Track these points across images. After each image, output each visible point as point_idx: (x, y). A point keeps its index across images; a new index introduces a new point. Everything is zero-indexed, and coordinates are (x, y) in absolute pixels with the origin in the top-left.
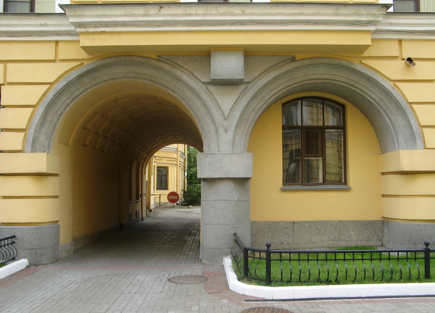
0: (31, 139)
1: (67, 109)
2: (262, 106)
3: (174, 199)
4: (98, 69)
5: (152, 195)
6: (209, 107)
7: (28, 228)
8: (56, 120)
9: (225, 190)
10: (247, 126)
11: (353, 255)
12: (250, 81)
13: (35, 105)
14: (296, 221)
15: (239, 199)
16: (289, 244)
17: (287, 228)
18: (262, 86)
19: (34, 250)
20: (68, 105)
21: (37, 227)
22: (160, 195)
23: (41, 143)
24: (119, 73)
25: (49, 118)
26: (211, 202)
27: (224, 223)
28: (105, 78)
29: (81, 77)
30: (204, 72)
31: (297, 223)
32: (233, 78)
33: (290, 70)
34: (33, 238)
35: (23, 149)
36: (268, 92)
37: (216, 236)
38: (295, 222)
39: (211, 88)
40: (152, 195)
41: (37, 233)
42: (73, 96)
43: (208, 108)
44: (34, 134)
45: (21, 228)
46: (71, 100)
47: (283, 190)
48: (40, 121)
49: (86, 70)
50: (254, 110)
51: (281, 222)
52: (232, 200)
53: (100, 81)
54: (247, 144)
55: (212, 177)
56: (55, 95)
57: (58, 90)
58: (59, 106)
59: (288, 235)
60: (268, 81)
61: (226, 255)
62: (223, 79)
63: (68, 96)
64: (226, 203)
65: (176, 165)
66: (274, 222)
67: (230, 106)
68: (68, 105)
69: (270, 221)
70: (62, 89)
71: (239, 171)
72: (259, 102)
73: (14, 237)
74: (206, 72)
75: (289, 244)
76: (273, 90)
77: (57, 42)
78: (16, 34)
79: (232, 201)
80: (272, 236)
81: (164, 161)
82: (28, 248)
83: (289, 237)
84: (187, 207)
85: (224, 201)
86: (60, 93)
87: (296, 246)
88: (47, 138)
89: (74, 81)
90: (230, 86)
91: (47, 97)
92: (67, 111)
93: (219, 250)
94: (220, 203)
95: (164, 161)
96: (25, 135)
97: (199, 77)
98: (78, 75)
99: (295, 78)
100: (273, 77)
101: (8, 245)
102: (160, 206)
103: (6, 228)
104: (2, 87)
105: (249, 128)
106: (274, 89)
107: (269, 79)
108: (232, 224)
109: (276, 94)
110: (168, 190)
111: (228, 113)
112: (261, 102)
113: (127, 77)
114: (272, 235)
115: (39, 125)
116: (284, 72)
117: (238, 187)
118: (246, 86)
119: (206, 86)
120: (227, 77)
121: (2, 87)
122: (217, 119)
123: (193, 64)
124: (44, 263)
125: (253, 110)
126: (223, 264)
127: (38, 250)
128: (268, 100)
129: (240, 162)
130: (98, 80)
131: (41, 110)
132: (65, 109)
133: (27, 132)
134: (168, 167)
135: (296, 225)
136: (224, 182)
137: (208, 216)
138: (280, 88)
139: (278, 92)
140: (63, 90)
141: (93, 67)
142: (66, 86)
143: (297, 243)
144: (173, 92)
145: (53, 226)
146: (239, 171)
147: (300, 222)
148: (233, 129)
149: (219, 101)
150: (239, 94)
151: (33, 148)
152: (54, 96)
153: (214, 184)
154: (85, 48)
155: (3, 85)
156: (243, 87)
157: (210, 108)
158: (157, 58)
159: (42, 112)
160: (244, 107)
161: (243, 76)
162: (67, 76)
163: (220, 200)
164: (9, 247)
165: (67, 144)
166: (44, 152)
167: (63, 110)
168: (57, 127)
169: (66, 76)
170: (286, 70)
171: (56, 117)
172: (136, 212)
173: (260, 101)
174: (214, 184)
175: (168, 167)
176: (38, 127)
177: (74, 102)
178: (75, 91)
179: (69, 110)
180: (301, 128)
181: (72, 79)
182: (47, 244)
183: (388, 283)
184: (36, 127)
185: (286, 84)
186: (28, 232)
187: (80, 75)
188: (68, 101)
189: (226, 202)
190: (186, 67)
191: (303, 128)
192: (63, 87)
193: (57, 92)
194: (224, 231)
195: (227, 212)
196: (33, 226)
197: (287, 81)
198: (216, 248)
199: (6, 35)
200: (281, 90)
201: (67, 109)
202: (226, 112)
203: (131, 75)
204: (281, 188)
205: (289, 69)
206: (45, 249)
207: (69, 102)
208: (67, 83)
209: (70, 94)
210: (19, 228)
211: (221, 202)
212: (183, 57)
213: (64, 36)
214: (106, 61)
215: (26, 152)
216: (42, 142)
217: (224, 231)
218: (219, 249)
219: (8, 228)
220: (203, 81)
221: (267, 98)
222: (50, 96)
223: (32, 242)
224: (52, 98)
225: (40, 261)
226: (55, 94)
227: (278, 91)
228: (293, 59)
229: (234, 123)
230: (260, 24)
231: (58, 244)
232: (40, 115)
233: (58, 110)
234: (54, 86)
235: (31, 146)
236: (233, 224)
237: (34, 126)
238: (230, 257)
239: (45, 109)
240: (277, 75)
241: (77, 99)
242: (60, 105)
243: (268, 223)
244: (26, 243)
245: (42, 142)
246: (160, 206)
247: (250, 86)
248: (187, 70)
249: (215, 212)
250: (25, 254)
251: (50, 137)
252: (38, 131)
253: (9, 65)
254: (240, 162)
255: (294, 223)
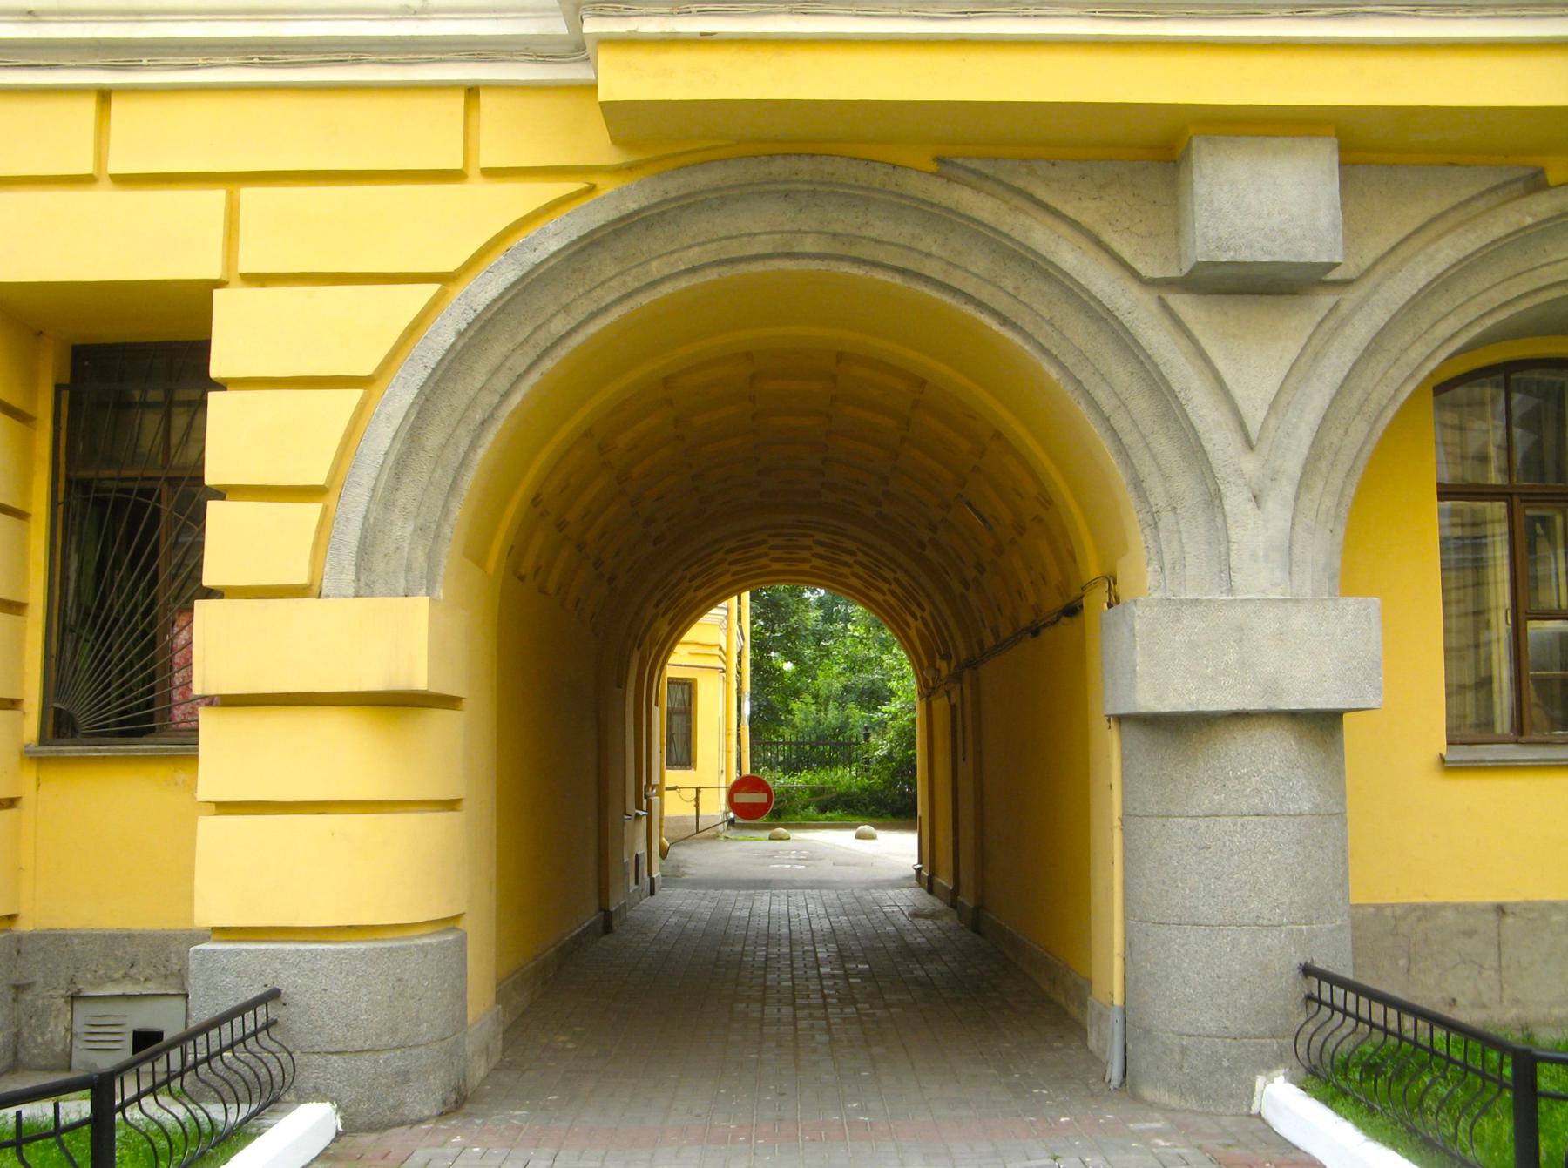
0: (352, 537)
1: (516, 399)
2: (1397, 391)
3: (754, 805)
4: (664, 213)
5: (668, 789)
6: (1177, 390)
7: (340, 952)
8: (463, 447)
9: (1260, 766)
10: (1337, 480)
11: (1319, 1007)
12: (1354, 277)
13: (370, 376)
14: (1511, 904)
15: (1316, 806)
16: (1484, 1006)
17: (1469, 933)
18: (1408, 297)
19: (367, 1055)
20: (520, 377)
21: (381, 945)
22: (698, 790)
23: (395, 552)
24: (759, 234)
25: (433, 438)
26: (1195, 821)
27: (1258, 917)
28: (692, 256)
29: (583, 249)
30: (1151, 235)
31: (1513, 913)
32: (1294, 260)
33: (1529, 227)
34: (365, 998)
35: (312, 581)
36: (1425, 329)
37: (1218, 977)
38: (1508, 910)
39: (1182, 304)
40: (668, 789)
41: (380, 975)
42: (543, 339)
43: (1176, 397)
44: (367, 511)
45: (306, 950)
46: (532, 356)
47: (1448, 766)
48: (396, 452)
49: (614, 215)
50: (1365, 409)
51: (1443, 906)
52: (1292, 813)
53: (667, 272)
54: (1337, 563)
55: (1202, 707)
56: (465, 330)
57: (480, 309)
58: (478, 385)
59: (1476, 963)
60: (1433, 276)
61: (1268, 1067)
62: (1252, 260)
63: (520, 338)
64: (1264, 824)
65: (724, 671)
66: (1414, 908)
67: (1271, 385)
68: (520, 377)
69: (1397, 904)
70: (499, 304)
71: (1324, 679)
72: (1385, 374)
73: (274, 995)
74: (1157, 235)
75: (1484, 1006)
76: (1445, 316)
77: (472, 91)
78: (284, 53)
79: (1290, 815)
80: (1408, 970)
81: (681, 656)
82: (340, 1047)
83: (1480, 973)
84: (767, 834)
85: (1258, 815)
86: (489, 321)
87: (1514, 1012)
88: (421, 529)
89: (551, 268)
90: (1267, 299)
91: (426, 337)
92: (513, 407)
93: (1234, 1042)
94: (1235, 824)
95: (681, 656)
96: (324, 513)
97: (1127, 255)
98: (574, 237)
99: (1536, 265)
100: (1454, 261)
101: (254, 1038)
102: (698, 832)
103: (239, 953)
104: (217, 293)
105: (1342, 490)
106: (1450, 313)
107: (1439, 270)
108: (1292, 923)
109: (1454, 336)
110: (695, 769)
111: (1261, 414)
112: (1391, 371)
113: (791, 255)
114: (1410, 962)
115: (391, 469)
116: (1501, 239)
117: (1313, 755)
118: (1336, 298)
119: (1160, 298)
120: (1269, 253)
121: (217, 293)
122: (1214, 445)
123: (1101, 198)
124: (412, 1117)
125: (1361, 406)
126: (1254, 1110)
127: (383, 1056)
128: (1421, 365)
129: (1329, 638)
130: (656, 269)
131: (400, 398)
132: (505, 396)
133: (332, 499)
134: (695, 680)
135: (1509, 920)
136: (1251, 732)
137: (1177, 886)
138: (1473, 312)
139: (1460, 330)
140: (502, 309)
141: (645, 203)
142: (515, 291)
143: (1516, 1001)
144: (1005, 321)
145: (445, 942)
146: (1324, 679)
147: (1529, 907)
148: (1288, 489)
149: (1222, 365)
150: (1309, 331)
151: (363, 579)
152: (461, 334)
153: (1207, 742)
154: (616, 114)
155: (219, 284)
156: (1325, 300)
157: (1183, 393)
158: (933, 167)
159: (407, 408)
160: (1334, 391)
161: (1340, 248)
162: (522, 244)
163: (1235, 815)
164: (261, 1046)
165: (480, 563)
166: (406, 596)
167: (496, 399)
168: (469, 481)
169: (516, 245)
170: (1511, 230)
171: (462, 431)
172: (637, 855)
173: (1389, 368)
174: (1205, 739)
175: (695, 680)
176: (384, 477)
177: (548, 364)
178: (553, 316)
179: (522, 402)
180: (1511, 495)
181: (546, 260)
182: (424, 1027)
183: (1329, 1101)
184: (377, 479)
185: (1499, 296)
186: (341, 973)
187: (580, 239)
188: (520, 362)
189: (1263, 819)
190: (1068, 209)
191: (1519, 494)
192: (502, 295)
193: (473, 316)
194: (1257, 955)
195: (1269, 869)
196: (362, 941)
197: (1503, 281)
198: (1219, 1034)
199: (239, 59)
200: (1477, 319)
201: (516, 399)
202: (1255, 416)
203: (809, 245)
204: (1441, 755)
205: (1523, 225)
206: (415, 1051)
207: (524, 368)
208: (521, 274)
209: (527, 330)
210: (298, 950)
211: (1243, 820)
212: (1054, 165)
213: (509, 61)
214: (701, 179)
215: (328, 596)
216: (398, 548)
217: (1257, 955)
218: (1235, 1039)
219: (246, 950)
220: (1148, 269)
221: (1419, 351)
222: (443, 335)
223: (357, 1018)
224: (453, 345)
225: (394, 1108)
226: (463, 326)
227: (1465, 323)
228: (1536, 183)
229: (1293, 464)
230: (1421, 13)
231: (462, 1020)
232: (396, 422)
233: (473, 402)
234: (457, 291)
235: (353, 568)
236: (1296, 923)
237: (366, 476)
238: (1284, 1074)
239: (417, 396)
240: (1469, 251)
241: (562, 351)
242: (485, 378)
243: (1388, 912)
244: (332, 1024)
245: (398, 548)
246: (698, 832)
247: (1352, 296)
248: (1074, 224)
249: (1216, 868)
250: (329, 1076)
251: (434, 526)
252: (384, 498)
253: (249, 195)
254: (1329, 638)
255: (1500, 909)
